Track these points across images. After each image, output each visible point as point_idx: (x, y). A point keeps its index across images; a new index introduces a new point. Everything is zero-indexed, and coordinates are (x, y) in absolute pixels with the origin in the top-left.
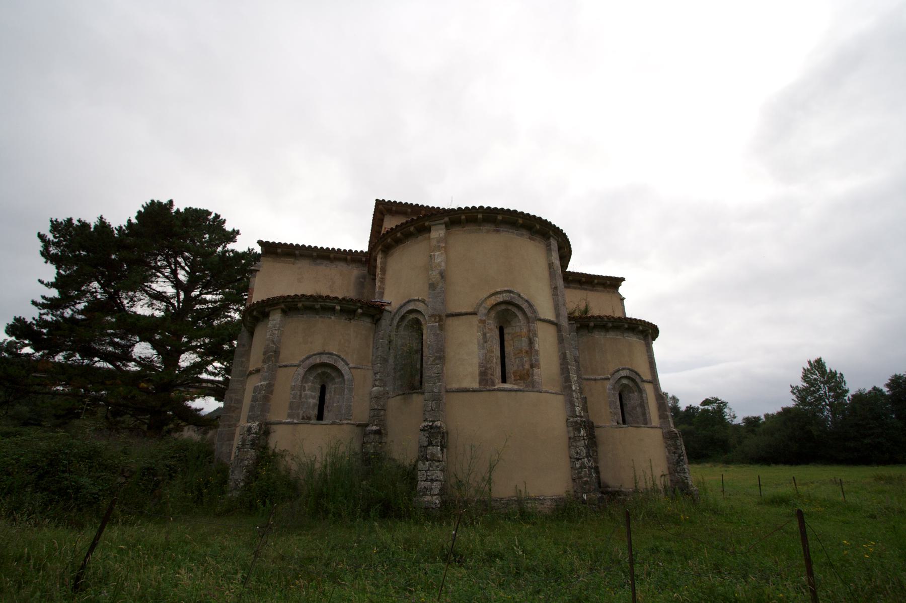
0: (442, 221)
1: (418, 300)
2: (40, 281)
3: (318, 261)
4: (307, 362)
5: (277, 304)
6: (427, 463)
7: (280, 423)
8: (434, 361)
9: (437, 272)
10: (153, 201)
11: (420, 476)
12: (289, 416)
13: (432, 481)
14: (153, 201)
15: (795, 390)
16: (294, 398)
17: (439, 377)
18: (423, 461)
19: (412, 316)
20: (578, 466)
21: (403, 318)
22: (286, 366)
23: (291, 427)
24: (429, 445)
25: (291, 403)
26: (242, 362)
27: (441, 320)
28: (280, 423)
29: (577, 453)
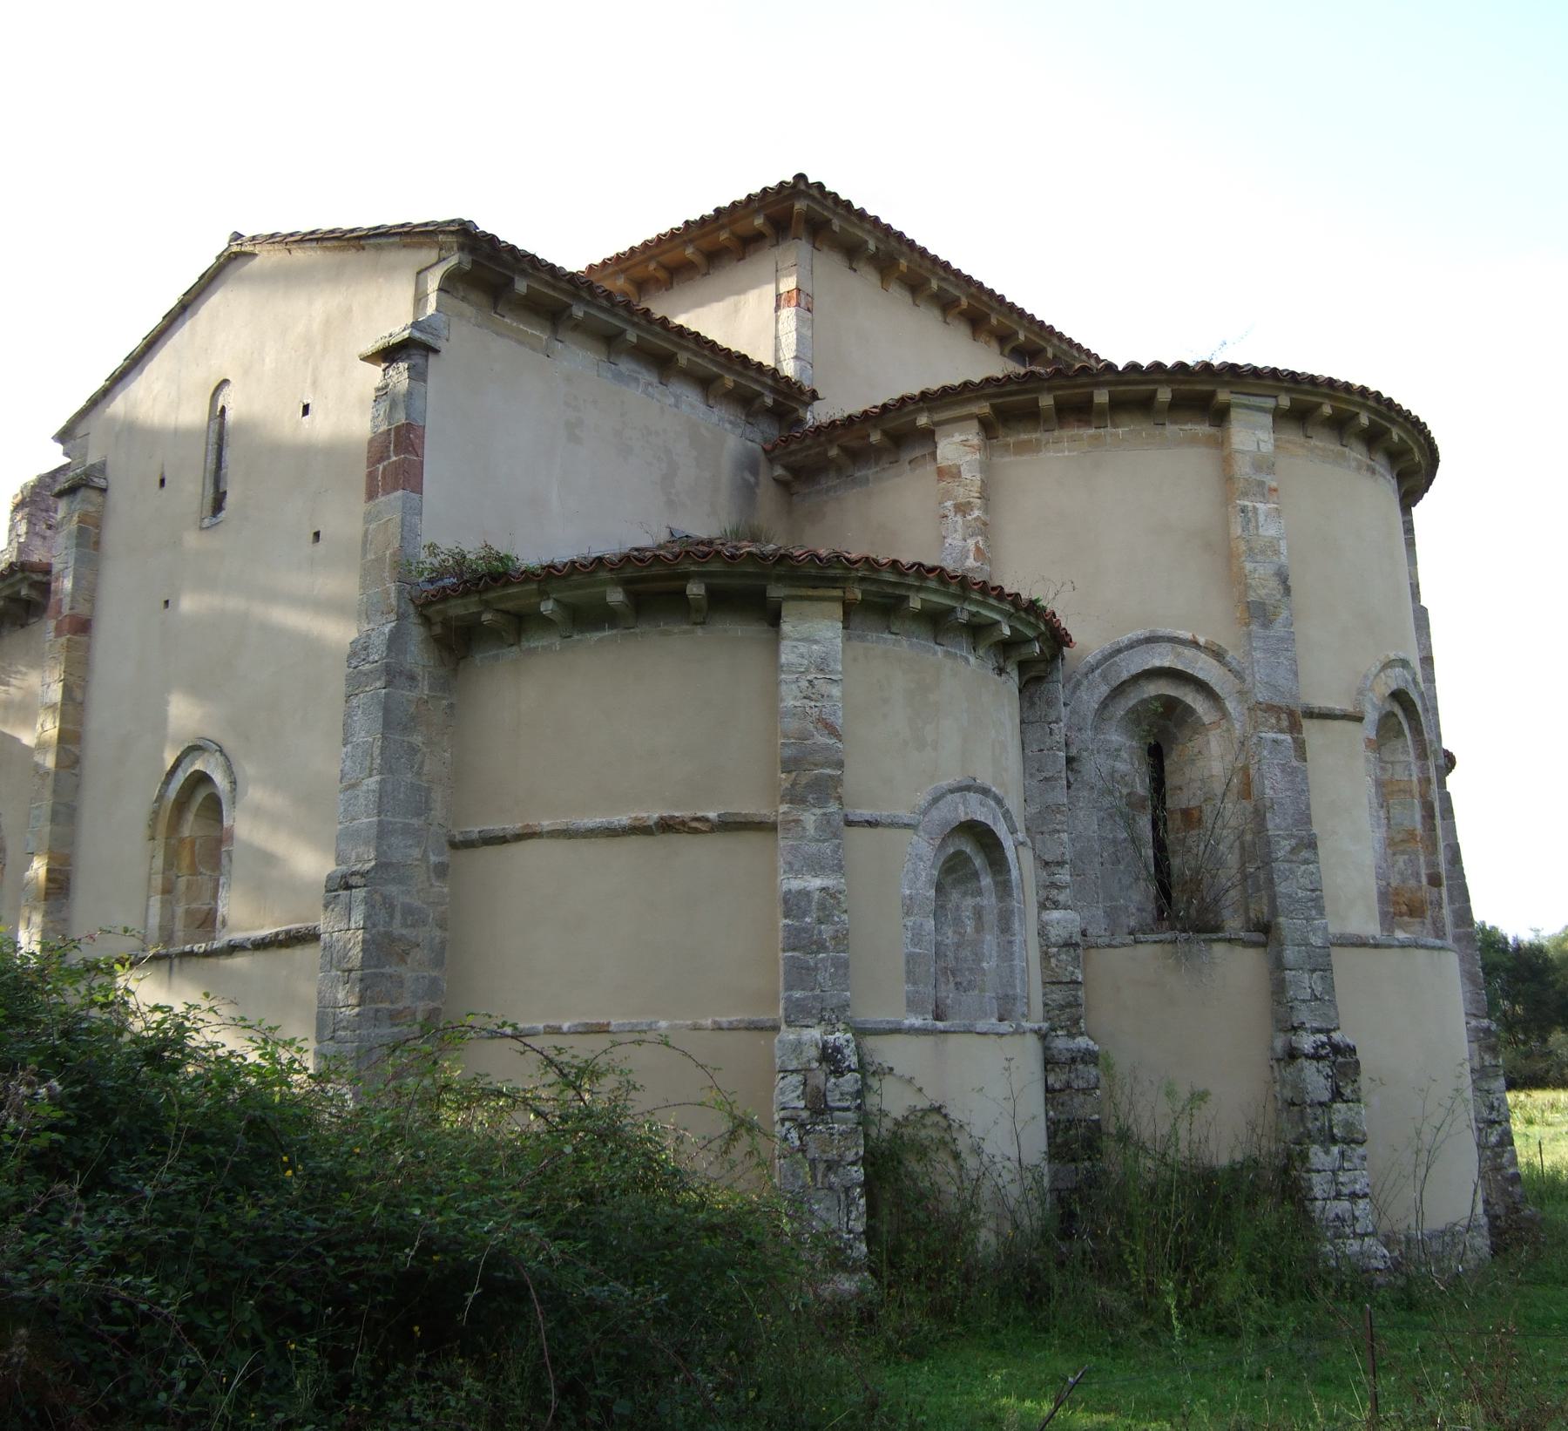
0: (1270, 403)
1: (1194, 644)
2: (225, 382)
3: (626, 366)
4: (934, 813)
5: (833, 582)
6: (1335, 1150)
7: (896, 1030)
8: (1293, 850)
9: (1271, 569)
10: (801, 177)
11: (1319, 1185)
12: (913, 1005)
13: (1354, 1196)
14: (801, 177)
15: (1483, 923)
16: (917, 939)
17: (1316, 902)
18: (1322, 1144)
19: (1152, 689)
20: (1493, 1139)
21: (1119, 690)
22: (871, 824)
23: (930, 1040)
24: (1333, 1100)
25: (910, 958)
26: (413, 750)
27: (1294, 727)
28: (896, 1030)
29: (1492, 1108)
